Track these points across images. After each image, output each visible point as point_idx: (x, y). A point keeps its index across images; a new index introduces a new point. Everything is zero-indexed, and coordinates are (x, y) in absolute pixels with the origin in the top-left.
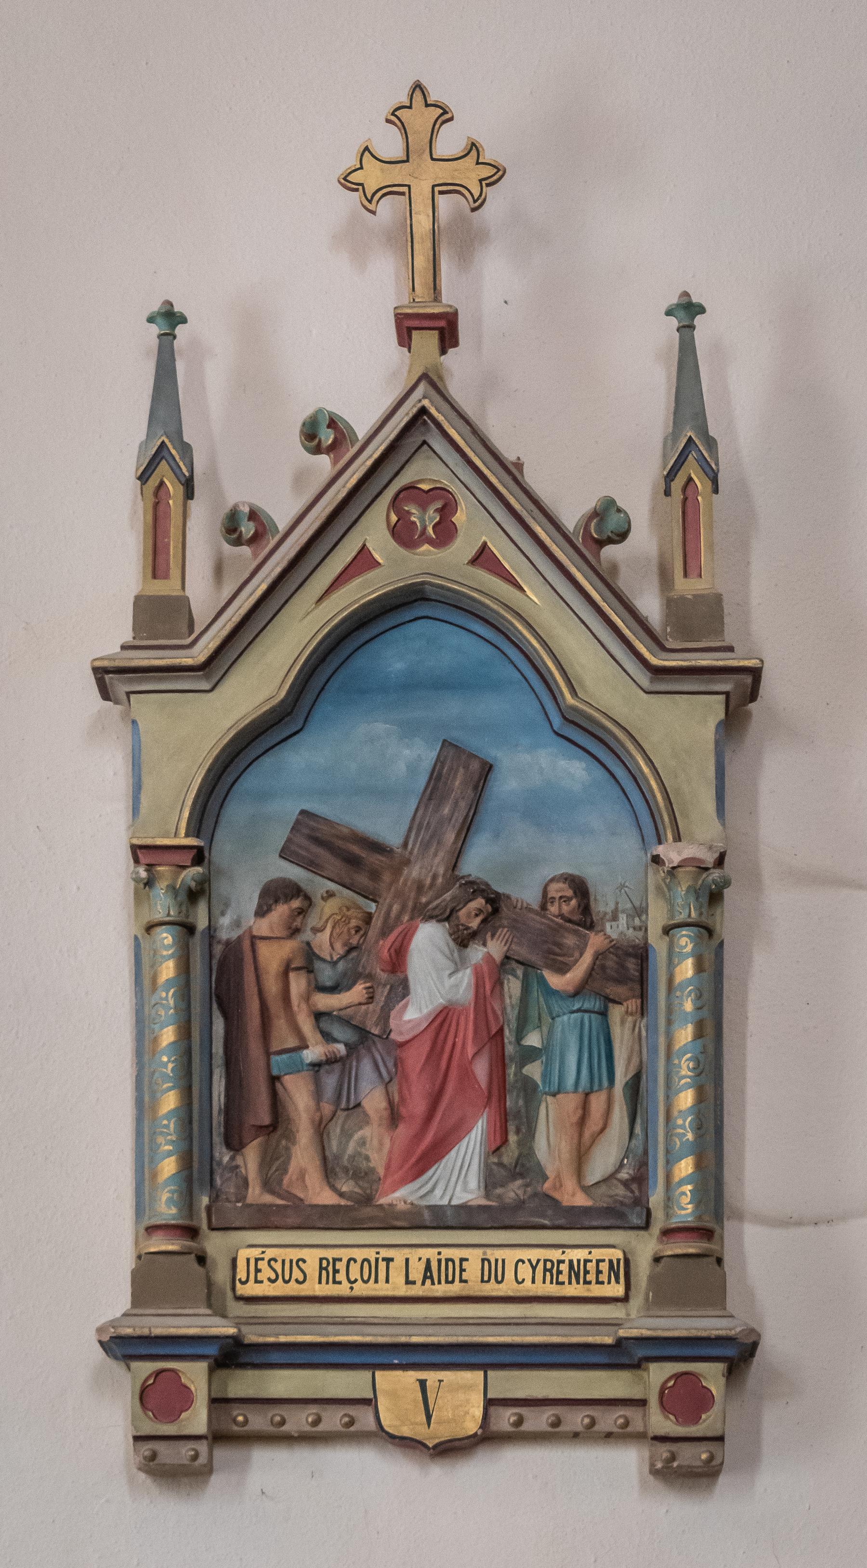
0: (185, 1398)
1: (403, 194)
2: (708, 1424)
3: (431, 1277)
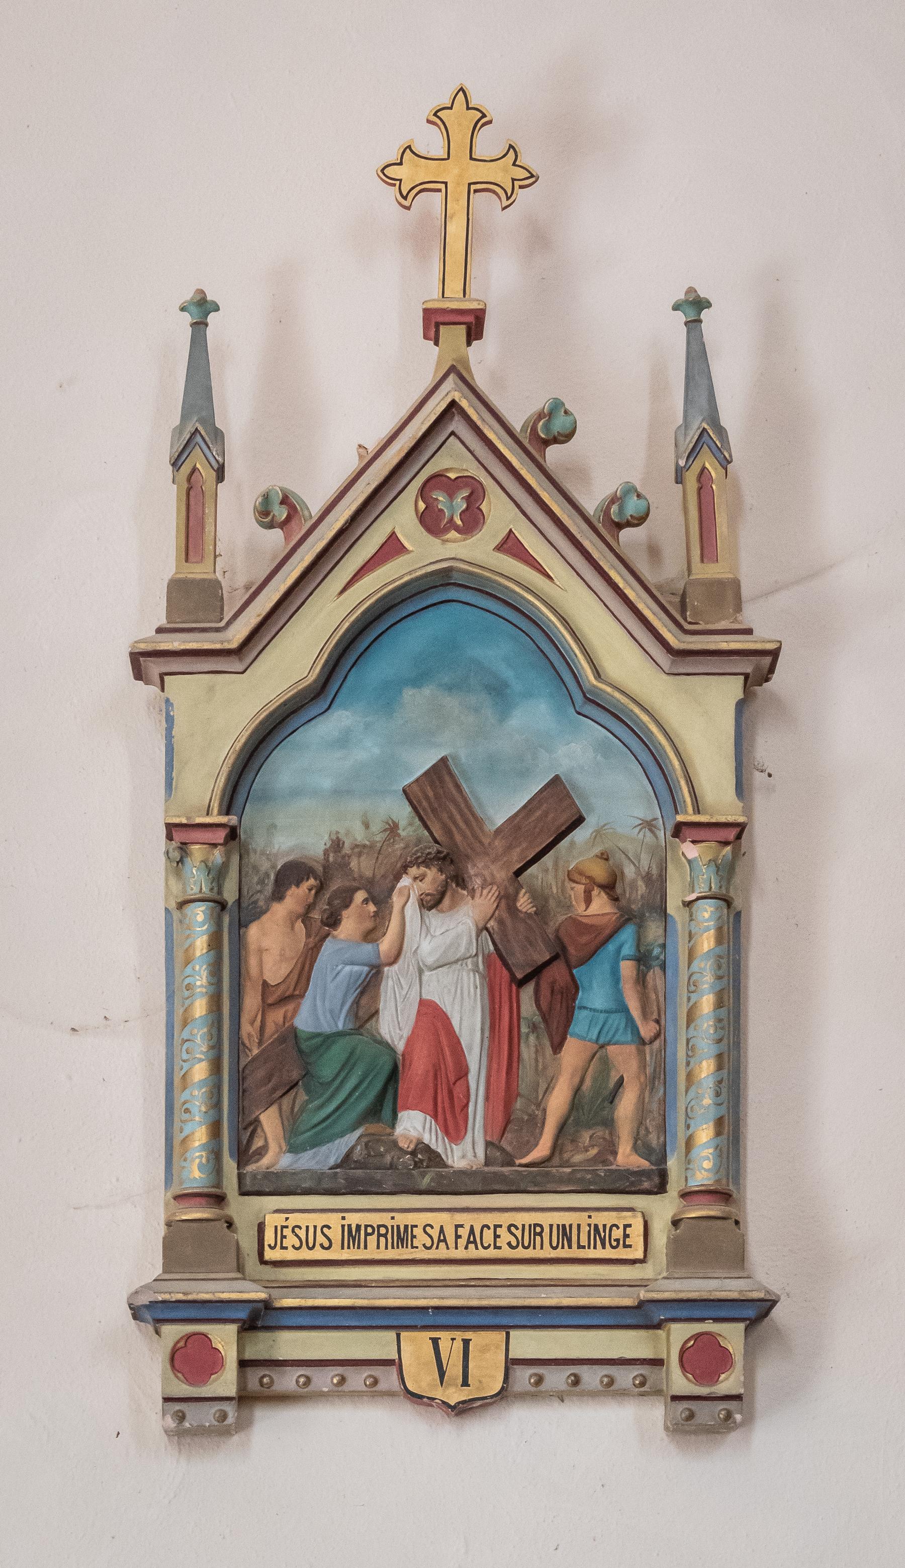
0: (213, 1362)
1: (439, 190)
2: (728, 1383)
3: (475, 1242)
